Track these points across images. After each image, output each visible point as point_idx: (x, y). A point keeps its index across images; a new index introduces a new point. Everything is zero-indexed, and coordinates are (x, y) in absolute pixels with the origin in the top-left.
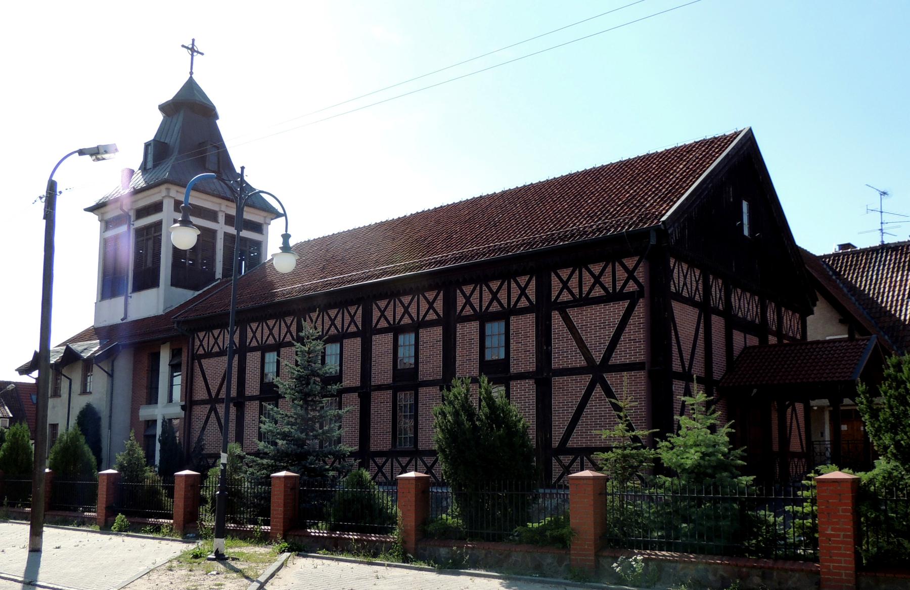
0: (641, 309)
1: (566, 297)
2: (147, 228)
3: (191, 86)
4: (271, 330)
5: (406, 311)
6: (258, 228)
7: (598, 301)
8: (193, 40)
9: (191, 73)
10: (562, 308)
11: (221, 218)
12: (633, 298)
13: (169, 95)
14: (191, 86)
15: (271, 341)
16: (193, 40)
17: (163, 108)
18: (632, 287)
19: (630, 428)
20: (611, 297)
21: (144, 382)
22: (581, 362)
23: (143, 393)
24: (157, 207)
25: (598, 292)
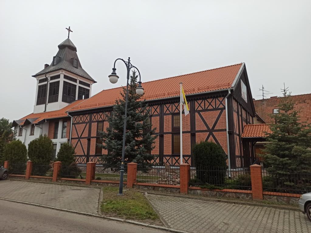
0: (88, 124)
1: (200, 109)
2: (43, 86)
3: (68, 40)
4: (101, 116)
5: (101, 116)
6: (89, 85)
7: (81, 123)
8: (69, 27)
9: (69, 37)
10: (199, 112)
11: (78, 81)
12: (87, 123)
13: (60, 42)
14: (68, 40)
15: (101, 119)
16: (69, 27)
17: (59, 47)
18: (87, 121)
19: (2, 147)
20: (83, 123)
21: (53, 132)
22: (206, 129)
23: (53, 135)
24: (58, 77)
25: (81, 121)
